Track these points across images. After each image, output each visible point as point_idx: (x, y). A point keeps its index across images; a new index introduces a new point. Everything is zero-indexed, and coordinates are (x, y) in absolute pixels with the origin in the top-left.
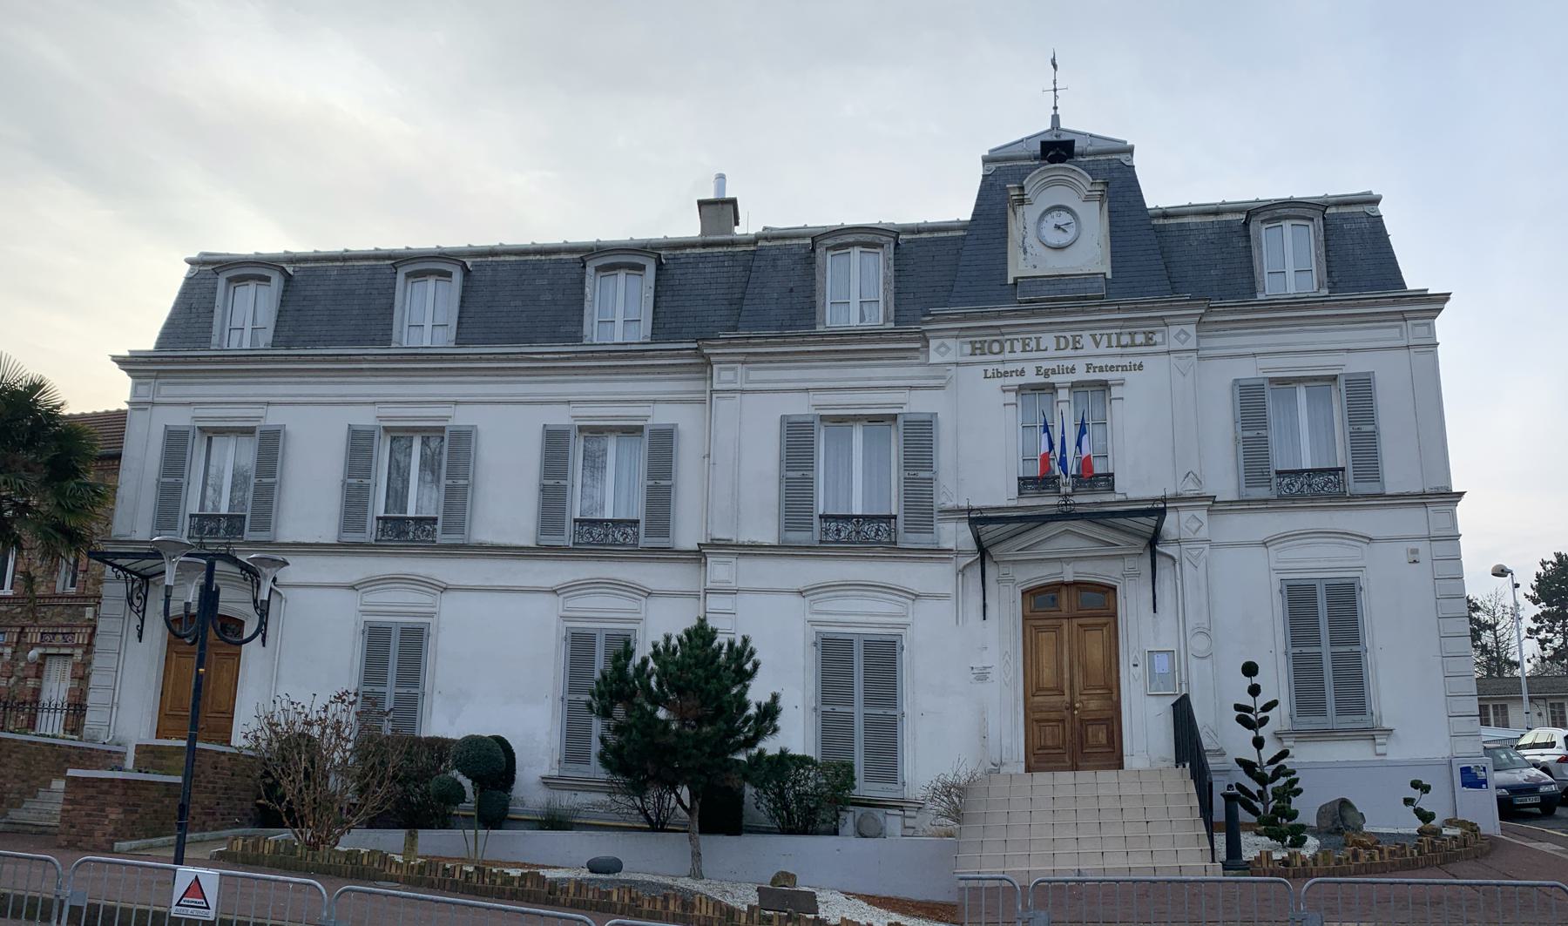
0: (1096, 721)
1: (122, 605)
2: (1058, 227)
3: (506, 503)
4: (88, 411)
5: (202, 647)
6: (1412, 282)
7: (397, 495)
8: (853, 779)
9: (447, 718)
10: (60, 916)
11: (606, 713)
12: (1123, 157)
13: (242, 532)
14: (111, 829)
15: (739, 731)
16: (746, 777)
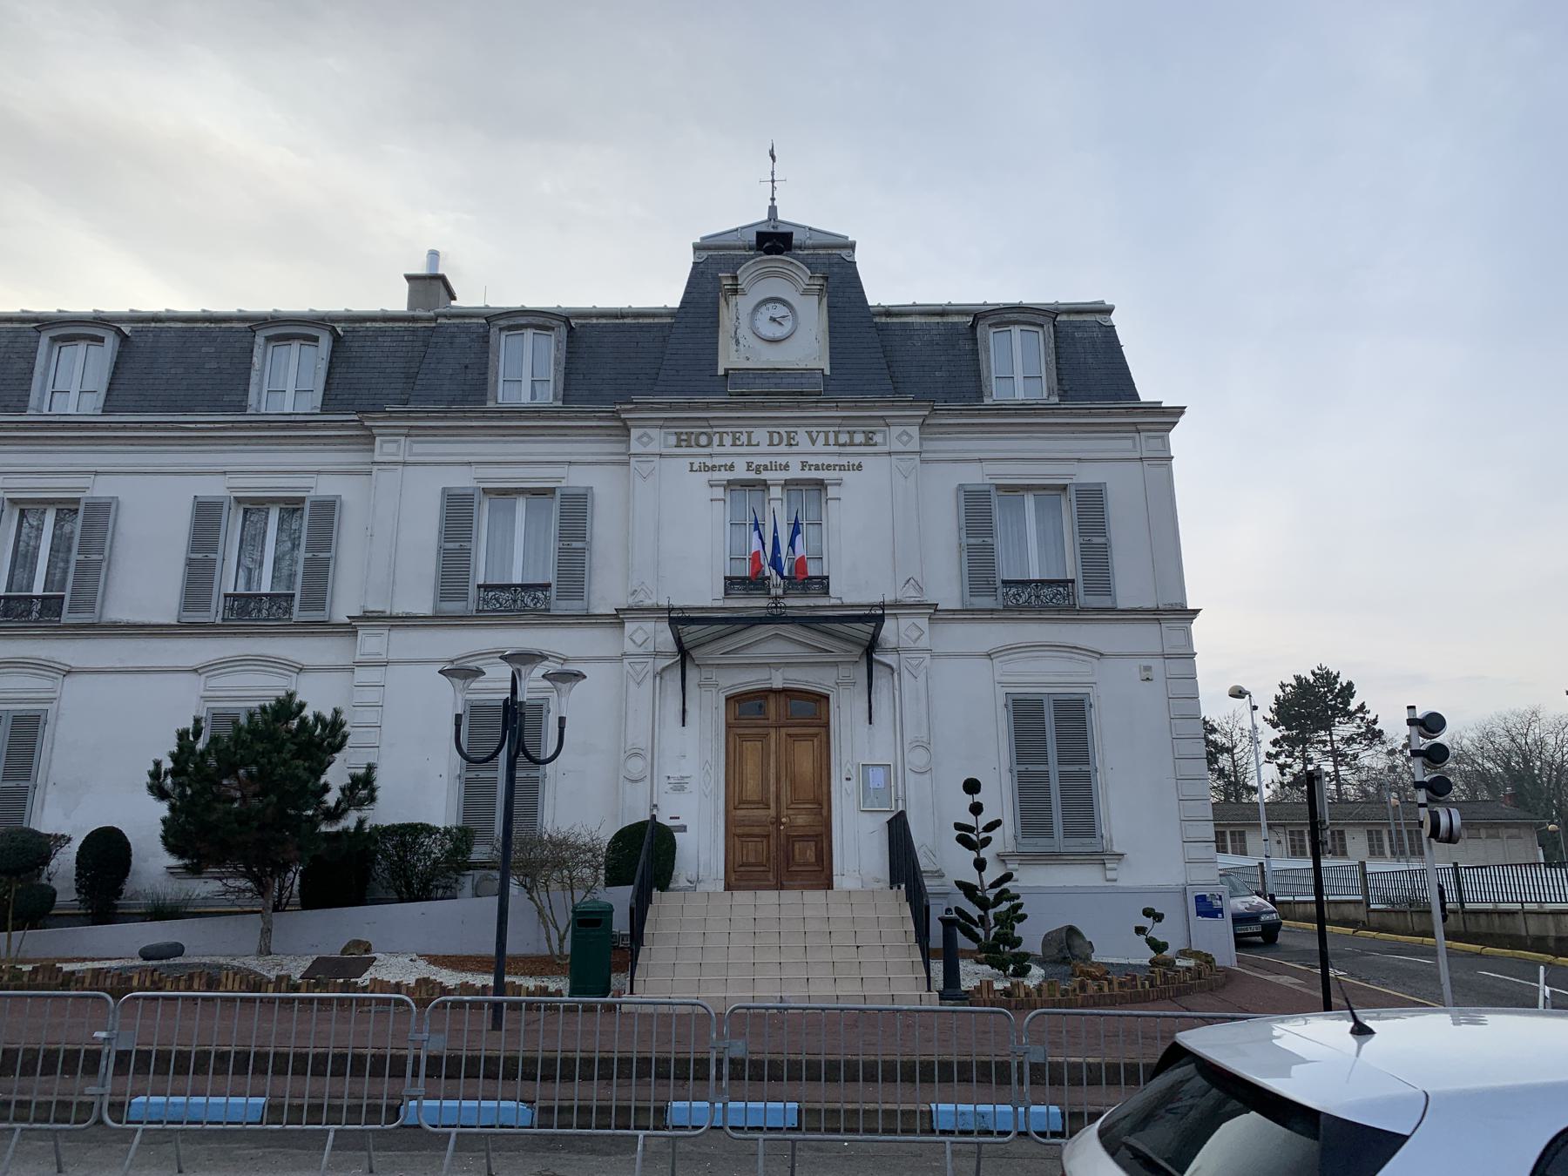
2: (773, 320)
3: (146, 578)
6: (1146, 394)
12: (844, 253)
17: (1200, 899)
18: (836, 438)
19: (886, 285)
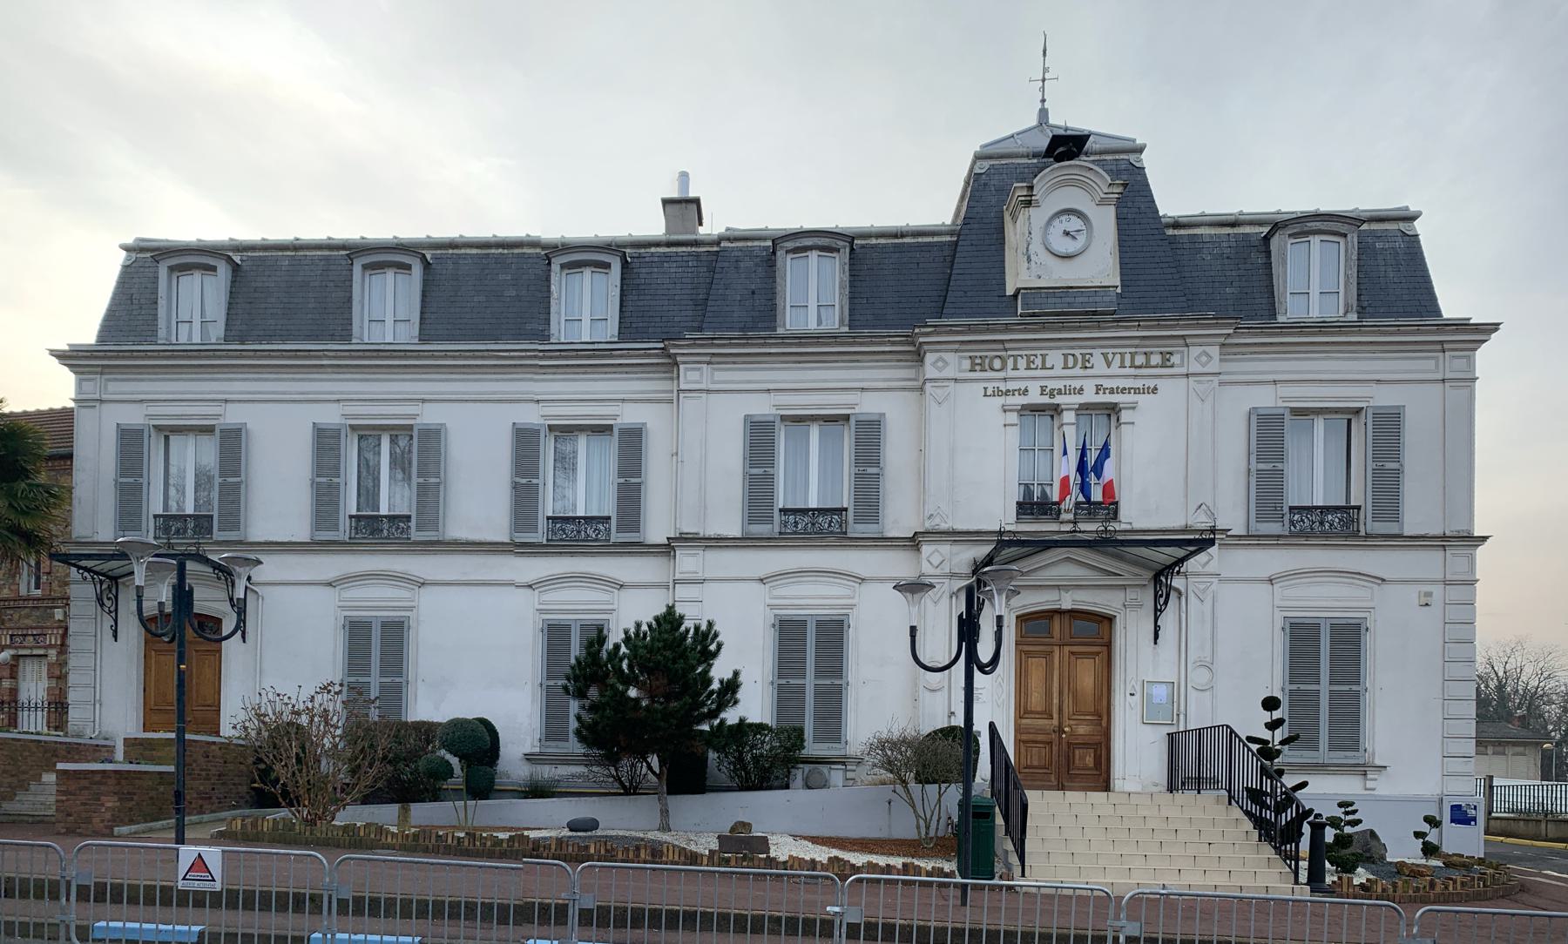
0: (1085, 745)
1: (92, 607)
2: (1067, 233)
3: (478, 500)
4: (31, 408)
5: (181, 645)
6: (1451, 306)
7: (368, 493)
8: (803, 740)
9: (429, 704)
10: (68, 895)
11: (581, 694)
12: (1132, 158)
13: (210, 532)
14: (108, 816)
15: (703, 704)
16: (709, 744)
17: (1456, 809)
18: (1133, 360)
19: (1177, 196)
